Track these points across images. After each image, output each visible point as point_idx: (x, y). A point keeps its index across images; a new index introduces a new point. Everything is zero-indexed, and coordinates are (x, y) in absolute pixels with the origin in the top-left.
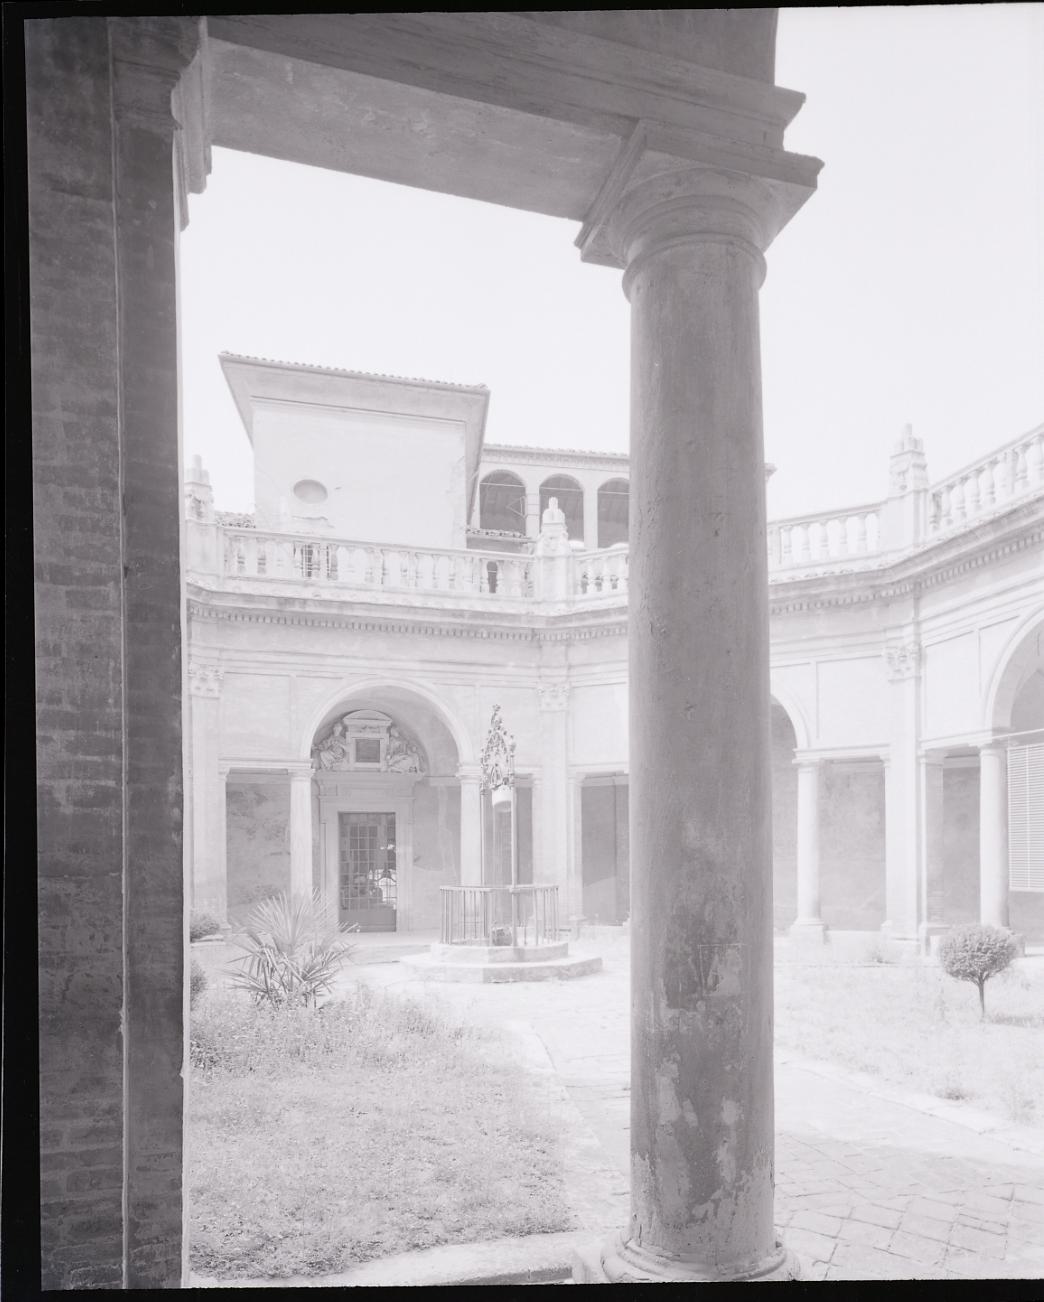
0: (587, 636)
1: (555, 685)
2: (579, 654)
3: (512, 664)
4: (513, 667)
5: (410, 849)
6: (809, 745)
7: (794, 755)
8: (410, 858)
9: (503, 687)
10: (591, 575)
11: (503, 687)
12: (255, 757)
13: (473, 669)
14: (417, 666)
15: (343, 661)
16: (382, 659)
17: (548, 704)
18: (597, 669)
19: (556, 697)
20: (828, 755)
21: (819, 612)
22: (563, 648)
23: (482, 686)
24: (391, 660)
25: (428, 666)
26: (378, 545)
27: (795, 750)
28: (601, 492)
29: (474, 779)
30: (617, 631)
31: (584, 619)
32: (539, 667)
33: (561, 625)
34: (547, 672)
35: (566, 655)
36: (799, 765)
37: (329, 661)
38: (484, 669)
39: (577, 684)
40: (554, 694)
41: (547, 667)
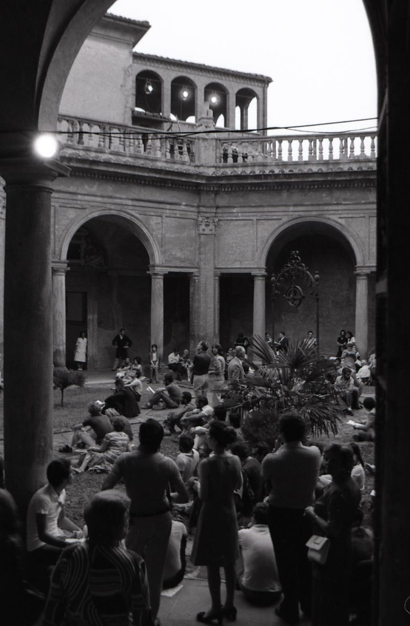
0: (230, 190)
1: (208, 218)
2: (222, 200)
3: (184, 203)
4: (185, 205)
5: (96, 316)
6: (364, 264)
7: (355, 269)
8: (96, 322)
9: (178, 218)
10: (230, 152)
11: (178, 218)
12: (235, 264)
13: (162, 206)
14: (130, 203)
15: (87, 198)
16: (111, 197)
17: (204, 230)
18: (235, 210)
19: (208, 225)
20: (224, 271)
21: (372, 189)
22: (213, 195)
23: (166, 217)
24: (116, 198)
25: (136, 203)
26: (109, 124)
27: (149, 266)
28: (238, 95)
29: (161, 275)
30: (249, 188)
31: (231, 180)
32: (198, 207)
33: (215, 182)
34: (203, 209)
35: (215, 201)
36: (358, 275)
37: (79, 197)
38: (168, 206)
39: (222, 219)
40: (208, 224)
41: (204, 206)
